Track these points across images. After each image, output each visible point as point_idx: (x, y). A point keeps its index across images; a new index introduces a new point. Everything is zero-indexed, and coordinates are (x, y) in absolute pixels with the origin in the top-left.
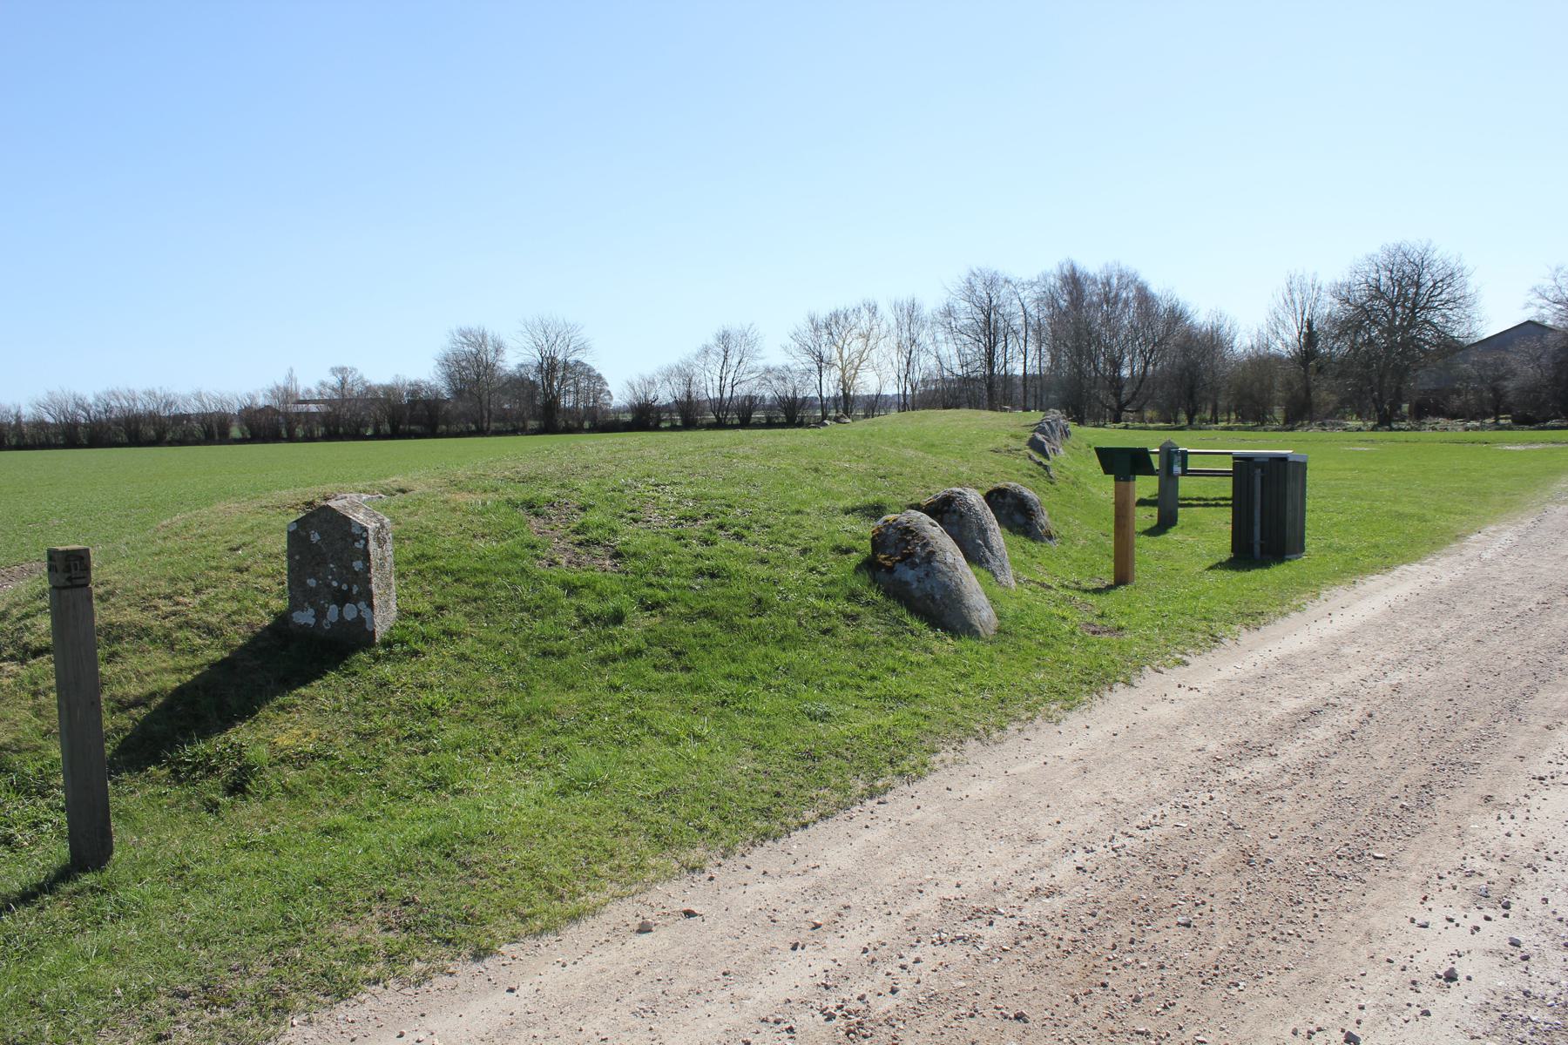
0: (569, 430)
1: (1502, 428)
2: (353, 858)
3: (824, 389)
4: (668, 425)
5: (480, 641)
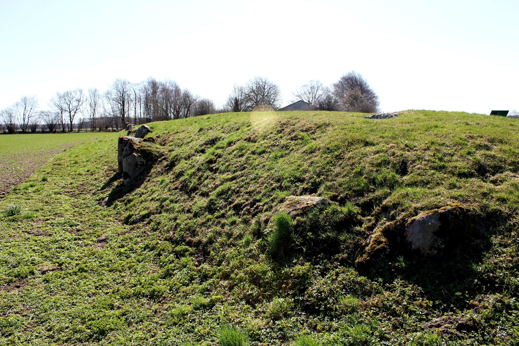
2: (498, 247)
3: (137, 114)
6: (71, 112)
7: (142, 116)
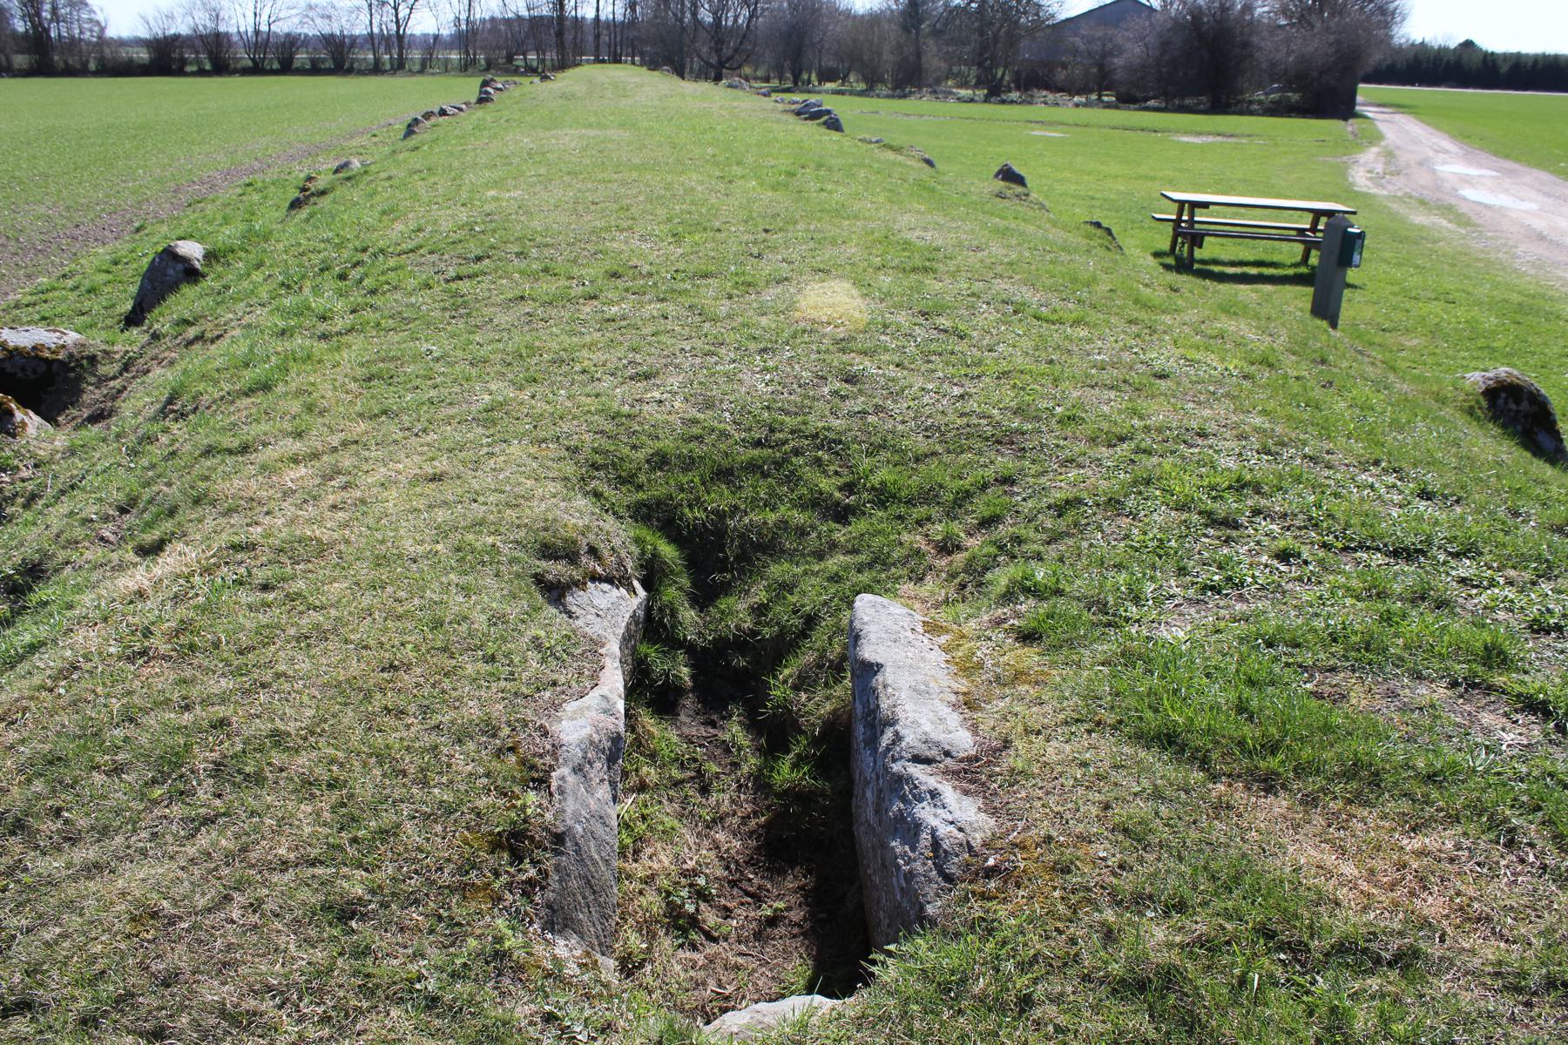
0: (69, 72)
1: (1108, 106)
4: (195, 68)
5: (596, 433)
6: (400, 8)
7: (619, 17)
